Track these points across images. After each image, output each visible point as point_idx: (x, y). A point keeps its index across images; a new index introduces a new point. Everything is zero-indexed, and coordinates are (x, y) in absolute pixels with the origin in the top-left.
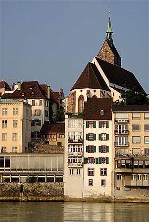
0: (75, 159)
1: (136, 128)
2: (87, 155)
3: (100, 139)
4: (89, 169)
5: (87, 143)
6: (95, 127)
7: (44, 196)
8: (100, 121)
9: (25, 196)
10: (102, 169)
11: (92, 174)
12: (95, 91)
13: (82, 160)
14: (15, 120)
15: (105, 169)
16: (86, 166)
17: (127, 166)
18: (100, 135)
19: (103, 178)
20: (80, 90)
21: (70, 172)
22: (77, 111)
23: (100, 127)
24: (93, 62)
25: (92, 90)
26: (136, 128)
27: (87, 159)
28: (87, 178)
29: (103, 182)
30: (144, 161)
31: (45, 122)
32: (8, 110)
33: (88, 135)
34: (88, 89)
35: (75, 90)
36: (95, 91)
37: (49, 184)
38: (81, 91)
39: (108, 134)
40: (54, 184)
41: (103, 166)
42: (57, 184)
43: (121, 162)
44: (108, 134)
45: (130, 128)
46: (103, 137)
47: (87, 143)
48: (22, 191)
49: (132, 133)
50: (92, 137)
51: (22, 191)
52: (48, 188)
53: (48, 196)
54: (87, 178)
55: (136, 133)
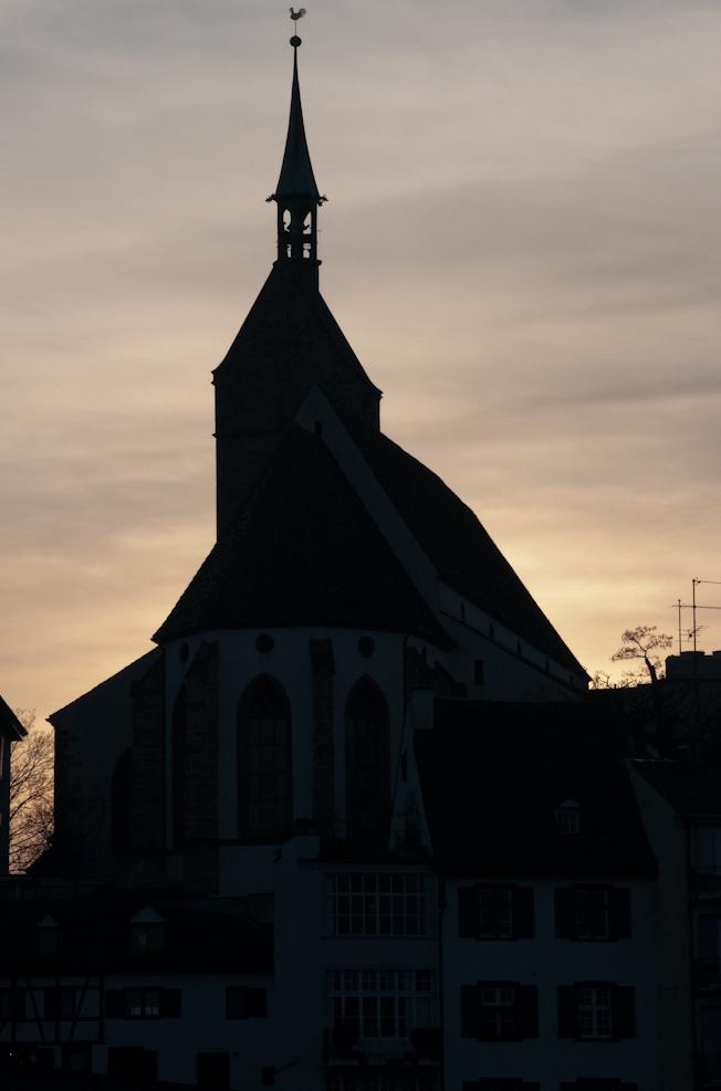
12: (366, 648)
36: (366, 648)
38: (265, 645)
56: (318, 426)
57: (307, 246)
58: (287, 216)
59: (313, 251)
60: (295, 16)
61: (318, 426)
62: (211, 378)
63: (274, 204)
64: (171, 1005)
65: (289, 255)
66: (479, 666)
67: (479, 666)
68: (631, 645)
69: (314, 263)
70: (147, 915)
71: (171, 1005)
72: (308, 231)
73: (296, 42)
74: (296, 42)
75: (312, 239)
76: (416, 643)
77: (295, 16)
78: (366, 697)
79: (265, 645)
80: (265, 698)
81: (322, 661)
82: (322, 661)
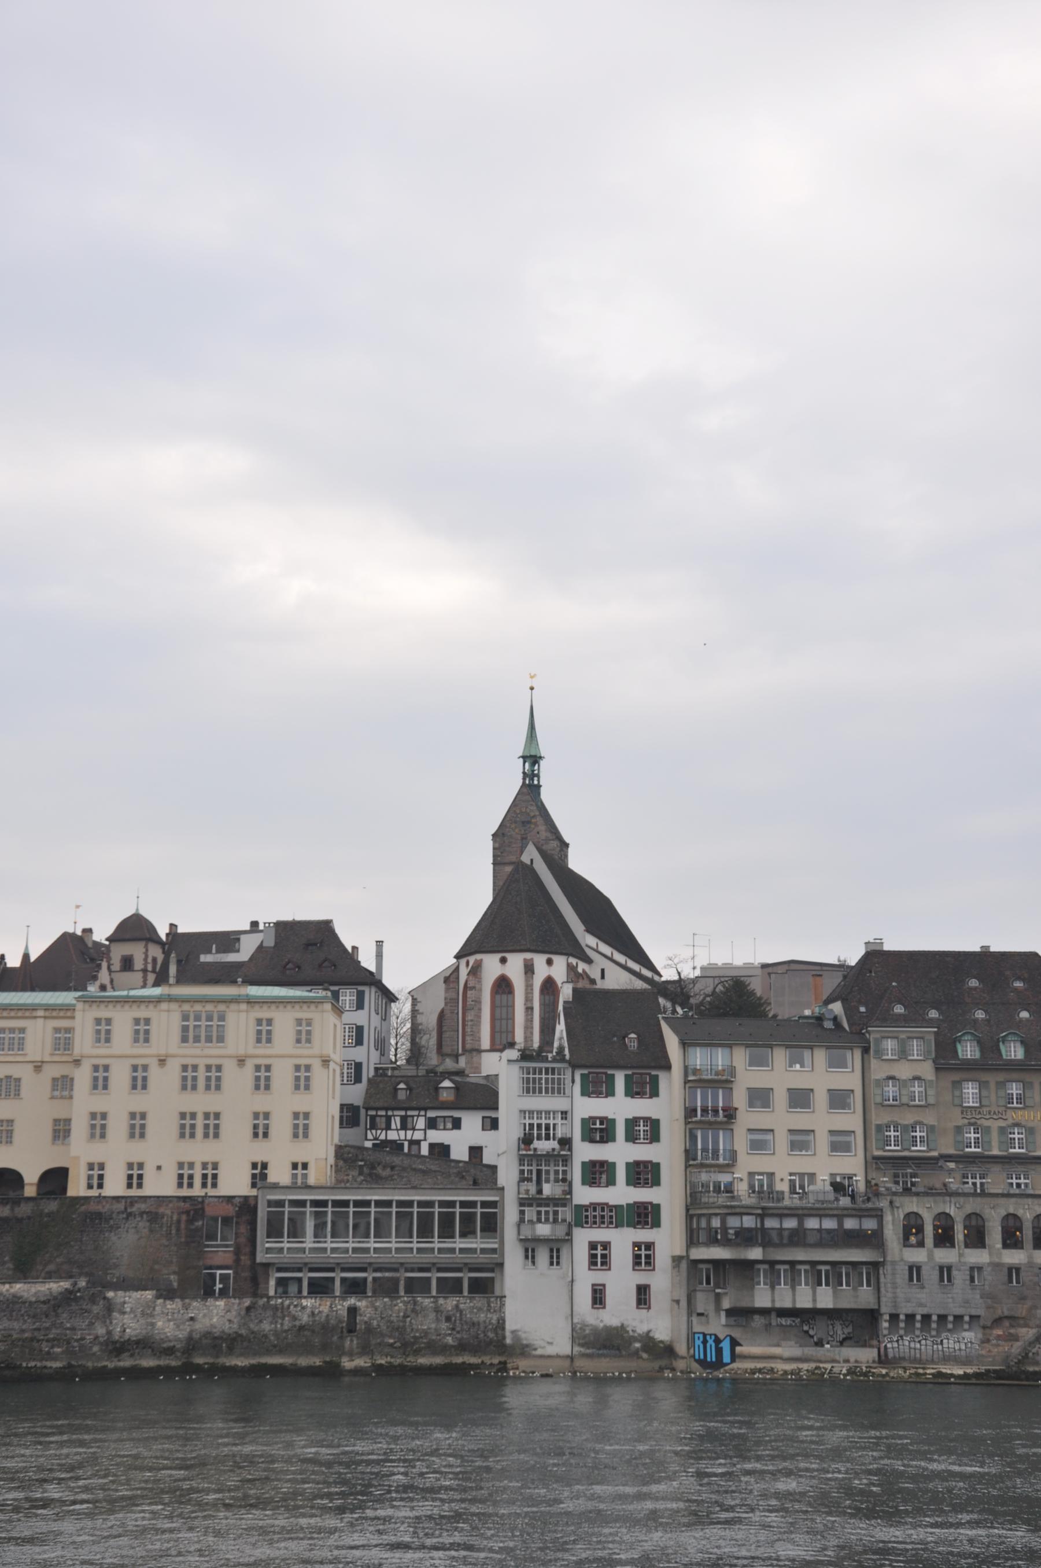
0: (543, 1209)
1: (760, 1097)
2: (584, 1195)
3: (632, 1137)
4: (593, 1246)
5: (584, 1152)
6: (611, 1093)
7: (434, 1347)
8: (629, 1072)
9: (365, 1350)
10: (637, 1245)
11: (602, 1264)
12: (549, 962)
13: (566, 1213)
14: (190, 1061)
15: (649, 1246)
16: (583, 1237)
17: (746, 1237)
18: (632, 1123)
19: (642, 1278)
20: (499, 956)
21: (552, 1257)
22: (1012, 1045)
23: (630, 1093)
24: (525, 859)
25: (539, 960)
26: (760, 1097)
27: (586, 1208)
28: (586, 1279)
29: (643, 1295)
30: (724, 1218)
31: (376, 1069)
32: (277, 1029)
33: (588, 1124)
34: (528, 956)
35: (478, 956)
36: (549, 962)
37: (449, 1303)
38: (503, 961)
39: (658, 1121)
40: (467, 1303)
41: (643, 1235)
42: (479, 1301)
43: (709, 1222)
44: (658, 1121)
45: (740, 1099)
46: (642, 1128)
47: (584, 1152)
48: (351, 1330)
49: (747, 1118)
50: (601, 1130)
51: (351, 1330)
52: (448, 1319)
53: (444, 1349)
54: (586, 1279)
55: (757, 1118)
56: (532, 860)
57: (536, 779)
58: (527, 765)
59: (539, 781)
60: (532, 677)
61: (532, 860)
62: (491, 838)
63: (521, 760)
64: (457, 1124)
65: (214, 946)
66: (603, 971)
67: (603, 971)
68: (670, 962)
69: (539, 786)
70: (447, 1083)
71: (457, 1124)
72: (536, 772)
73: (532, 689)
74: (532, 689)
75: (538, 776)
76: (573, 961)
77: (532, 677)
78: (549, 985)
79: (503, 961)
80: (503, 985)
81: (529, 969)
82: (529, 969)
